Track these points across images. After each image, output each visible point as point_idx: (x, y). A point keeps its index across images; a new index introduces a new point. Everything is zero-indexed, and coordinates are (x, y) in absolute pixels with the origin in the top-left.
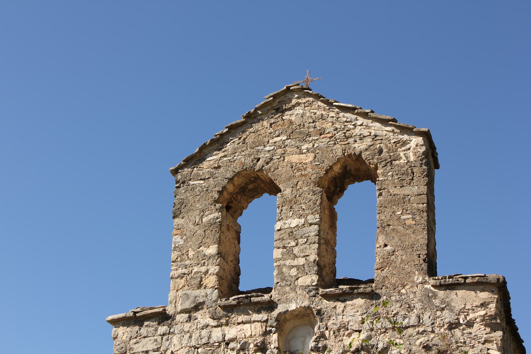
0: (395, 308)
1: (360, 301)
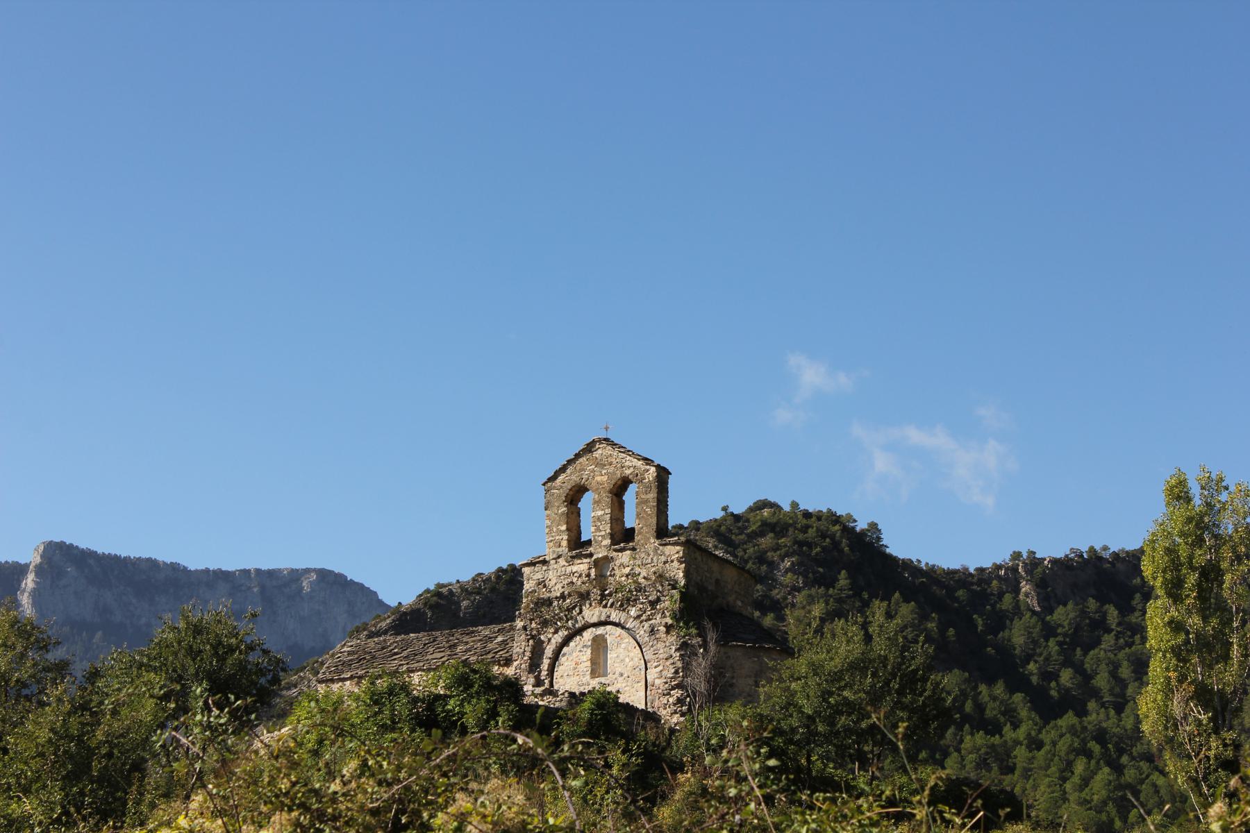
0: (643, 555)
1: (628, 552)
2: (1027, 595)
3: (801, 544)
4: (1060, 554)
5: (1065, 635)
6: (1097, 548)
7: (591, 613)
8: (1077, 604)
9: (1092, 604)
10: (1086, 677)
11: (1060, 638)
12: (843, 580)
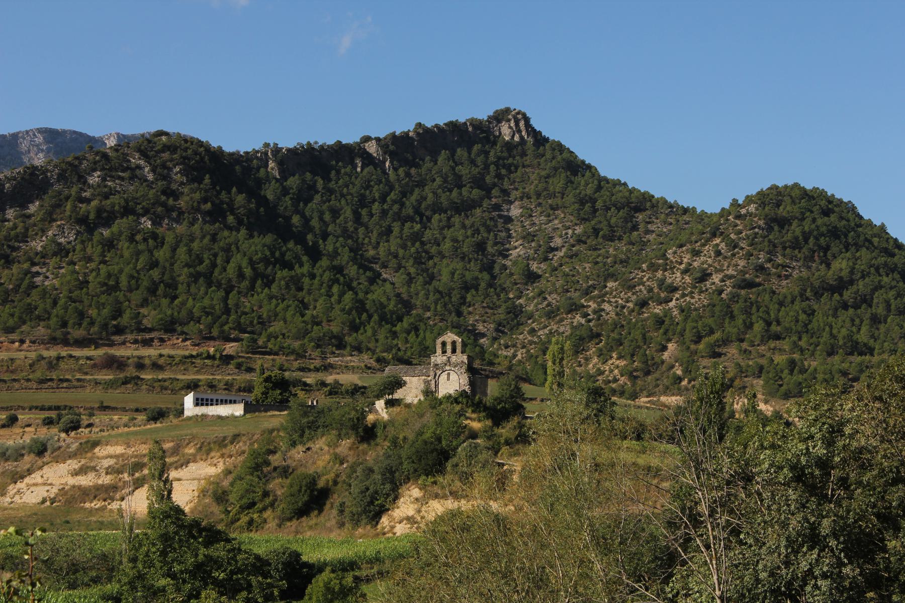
2: (272, 169)
3: (185, 158)
4: (291, 146)
5: (294, 194)
6: (312, 142)
7: (447, 368)
8: (300, 175)
9: (308, 176)
10: (306, 220)
11: (291, 196)
12: (207, 179)
